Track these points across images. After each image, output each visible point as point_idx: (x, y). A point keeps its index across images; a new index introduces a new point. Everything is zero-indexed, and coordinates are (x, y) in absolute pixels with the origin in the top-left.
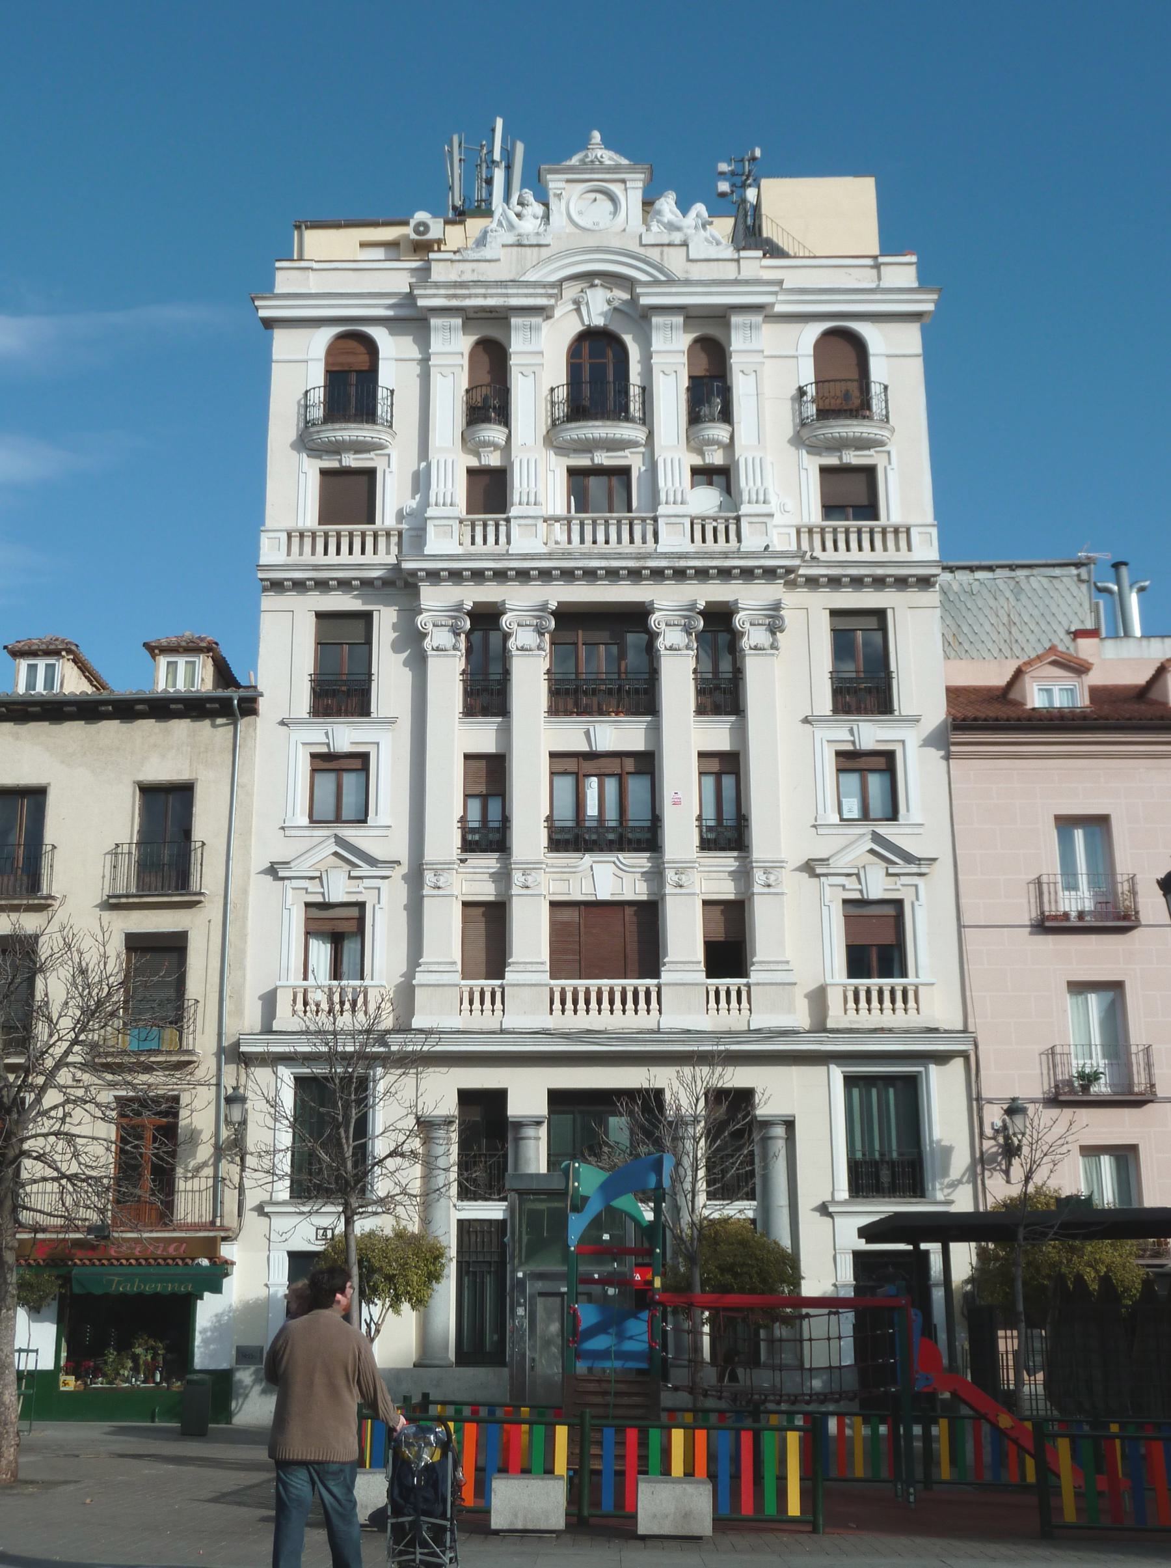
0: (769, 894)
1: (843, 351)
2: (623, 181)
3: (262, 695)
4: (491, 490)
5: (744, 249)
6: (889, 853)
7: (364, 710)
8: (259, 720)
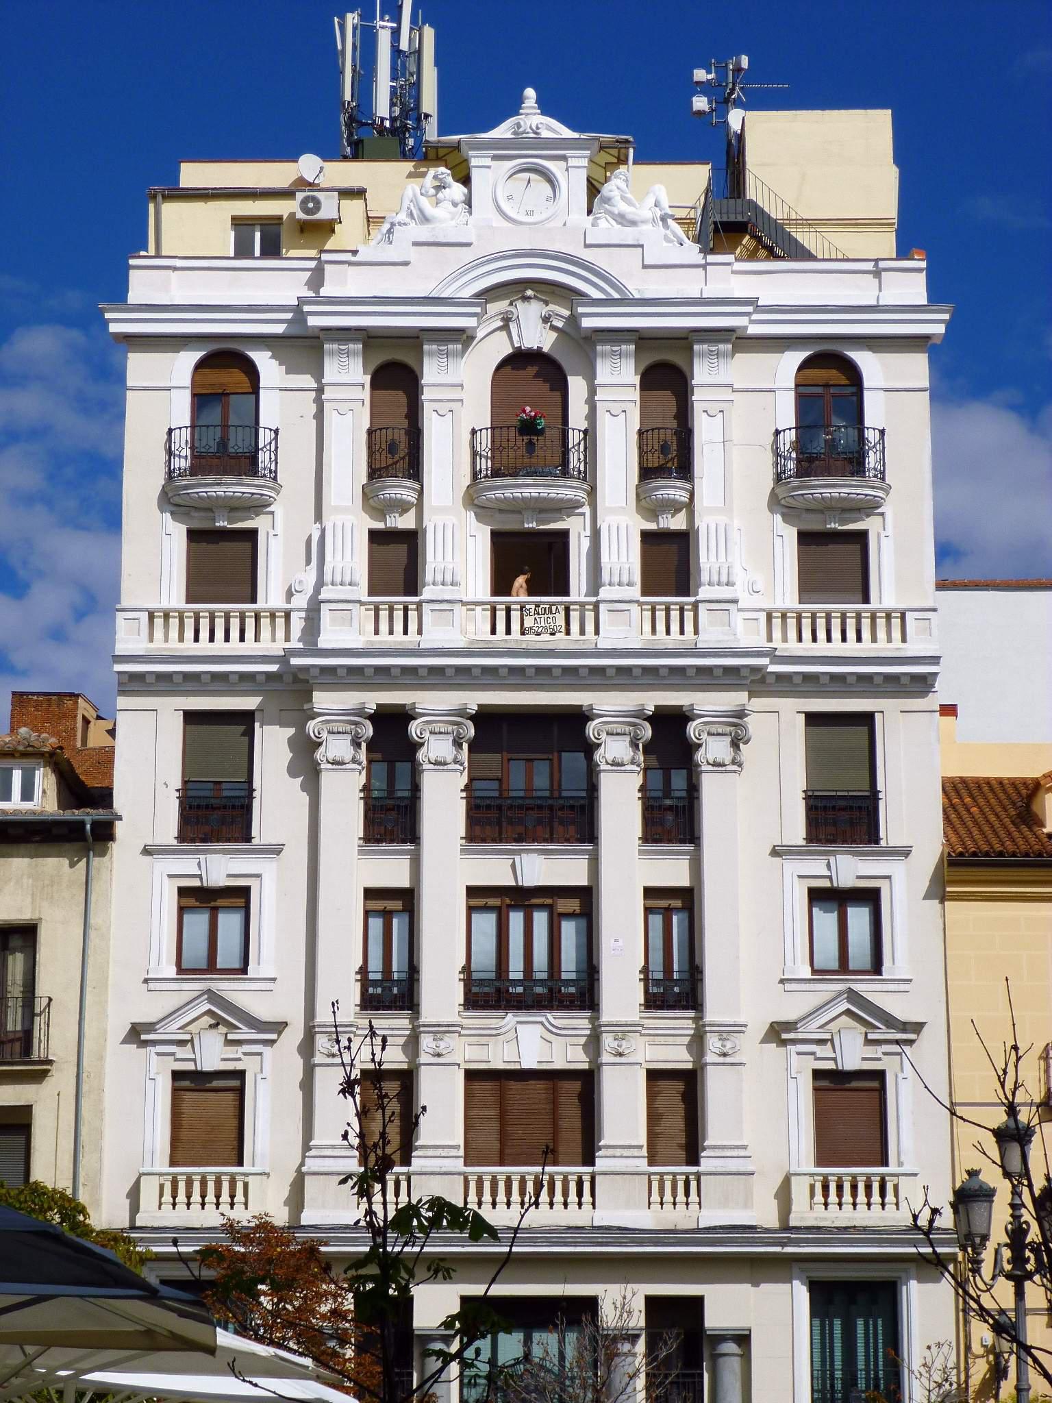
0: (723, 1064)
1: (830, 385)
3: (120, 818)
4: (398, 561)
5: (712, 251)
6: (867, 1014)
8: (115, 847)
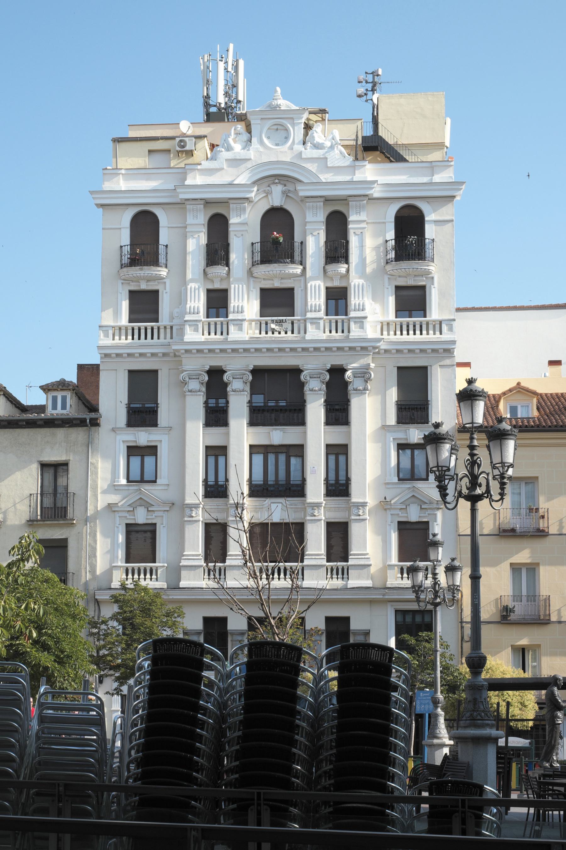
2: (292, 118)
4: (218, 302)
7: (155, 424)
